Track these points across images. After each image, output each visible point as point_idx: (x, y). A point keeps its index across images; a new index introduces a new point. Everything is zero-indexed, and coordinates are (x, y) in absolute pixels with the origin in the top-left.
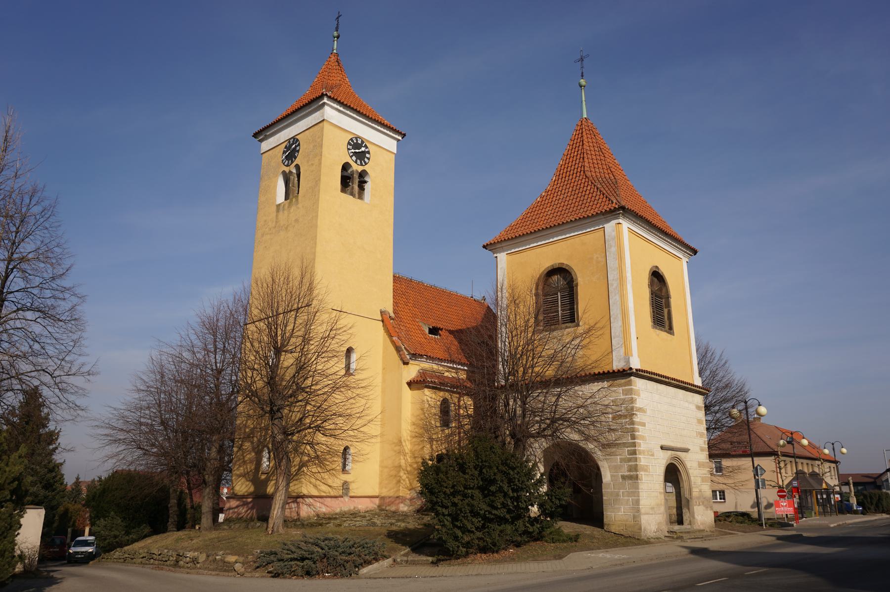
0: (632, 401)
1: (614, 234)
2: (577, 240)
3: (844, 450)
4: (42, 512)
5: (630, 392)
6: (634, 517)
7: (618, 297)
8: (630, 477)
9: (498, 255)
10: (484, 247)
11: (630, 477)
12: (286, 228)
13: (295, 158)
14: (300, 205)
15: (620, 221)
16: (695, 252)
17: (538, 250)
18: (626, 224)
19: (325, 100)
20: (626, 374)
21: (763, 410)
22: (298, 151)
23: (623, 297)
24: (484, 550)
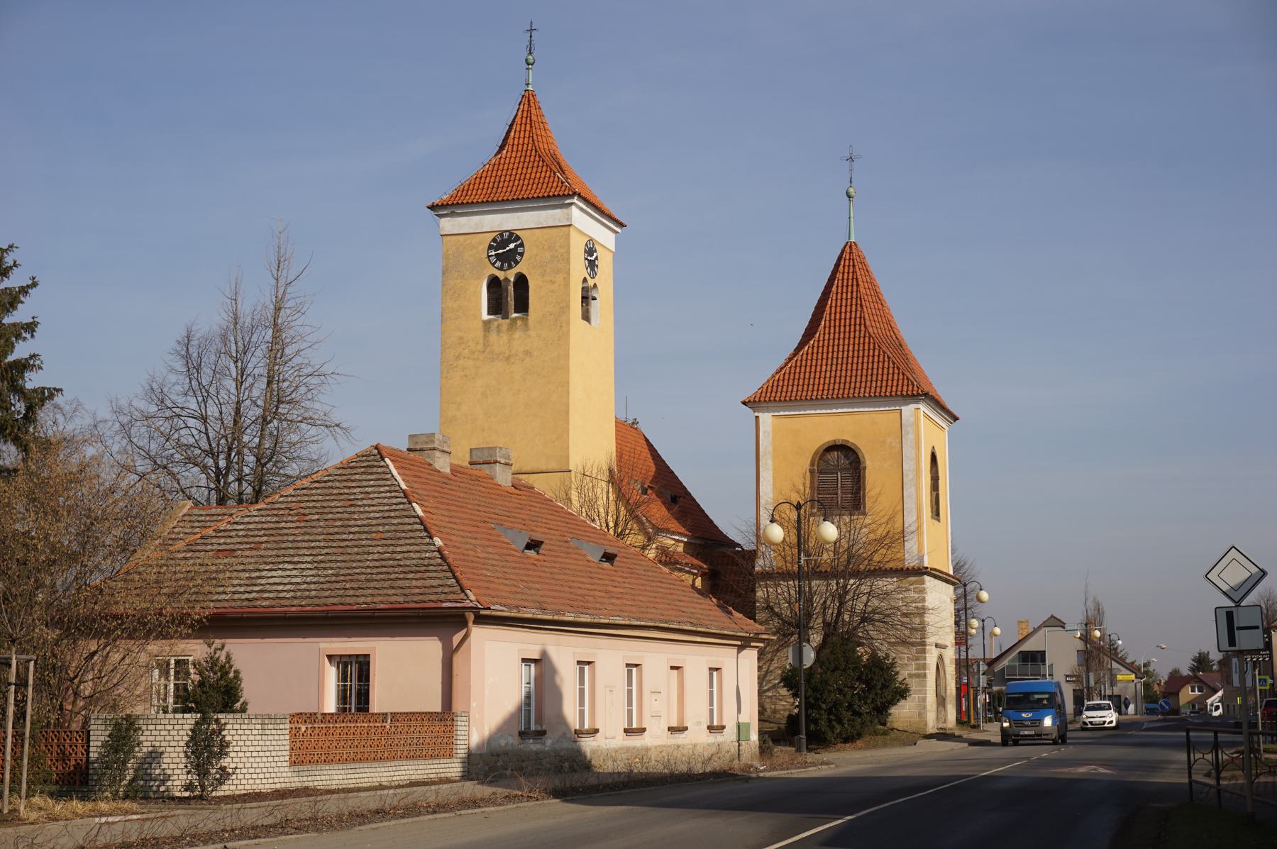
0: (924, 600)
1: (912, 419)
2: (866, 417)
3: (997, 631)
4: (439, 710)
5: (923, 591)
6: (920, 714)
7: (913, 490)
8: (918, 676)
9: (760, 415)
10: (744, 403)
11: (918, 676)
12: (508, 359)
13: (517, 263)
14: (532, 333)
15: (920, 406)
16: (956, 419)
17: (817, 419)
18: (923, 408)
19: (575, 200)
20: (921, 572)
21: (984, 595)
22: (522, 254)
23: (918, 489)
24: (846, 741)
